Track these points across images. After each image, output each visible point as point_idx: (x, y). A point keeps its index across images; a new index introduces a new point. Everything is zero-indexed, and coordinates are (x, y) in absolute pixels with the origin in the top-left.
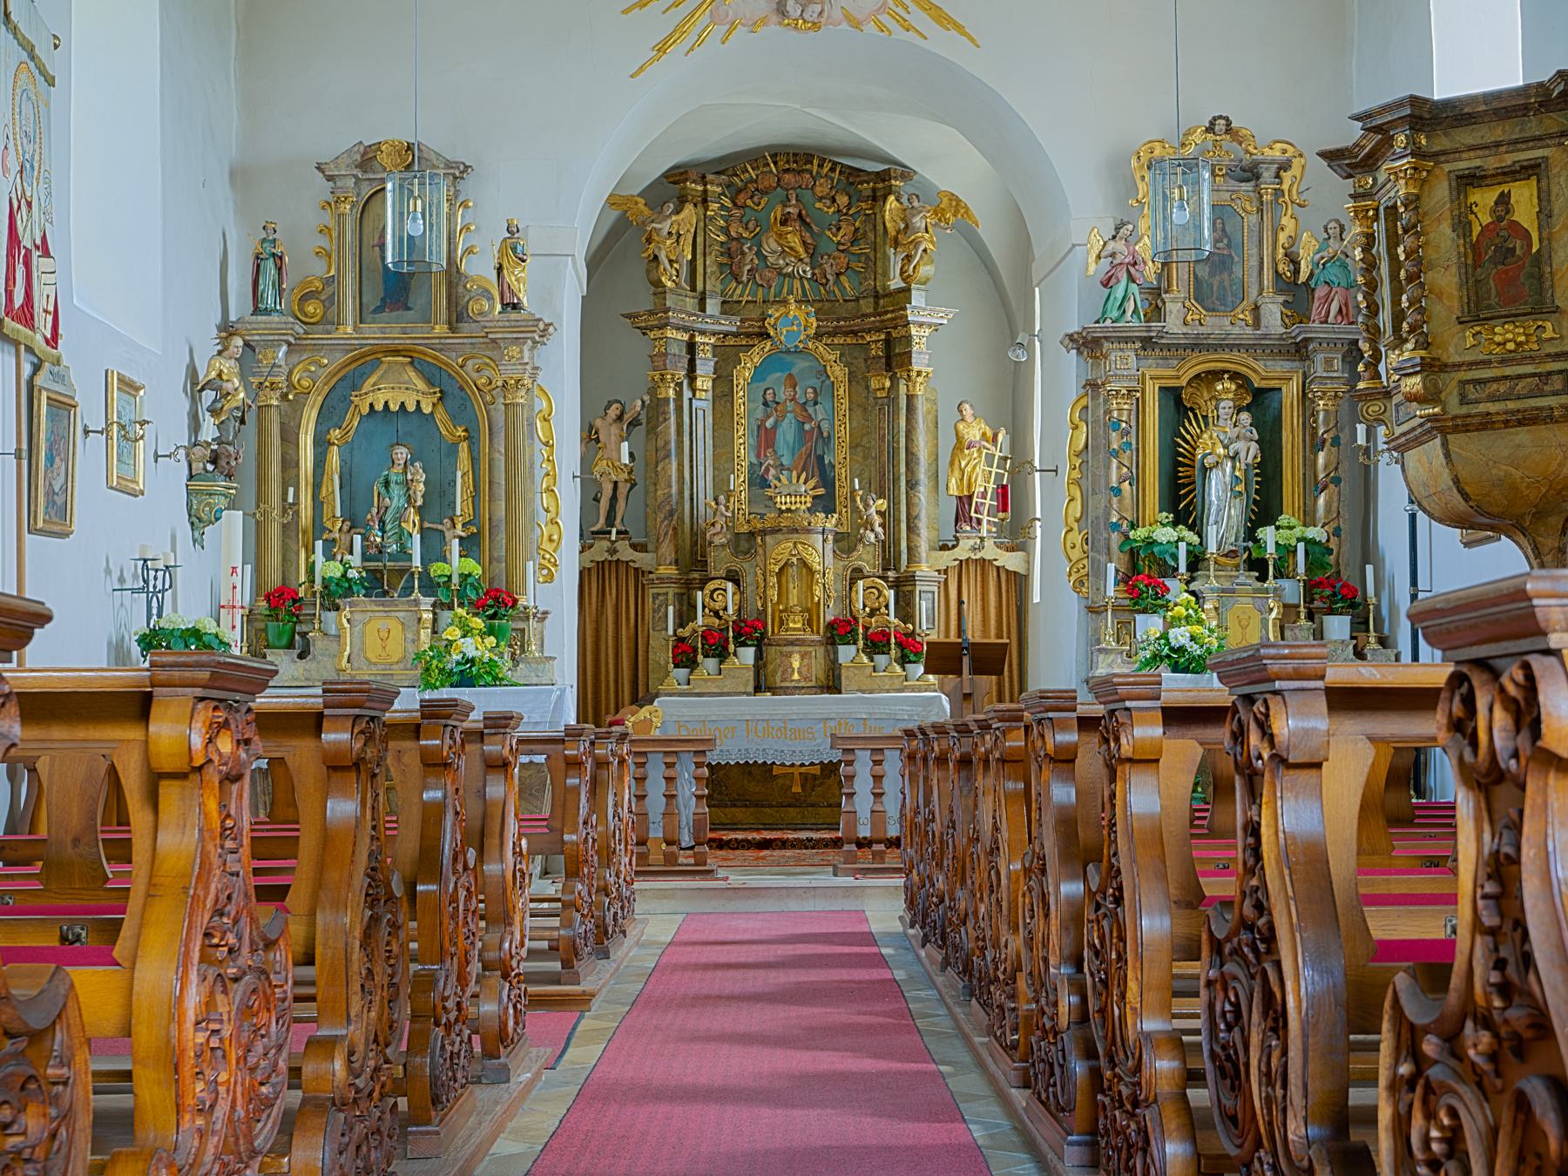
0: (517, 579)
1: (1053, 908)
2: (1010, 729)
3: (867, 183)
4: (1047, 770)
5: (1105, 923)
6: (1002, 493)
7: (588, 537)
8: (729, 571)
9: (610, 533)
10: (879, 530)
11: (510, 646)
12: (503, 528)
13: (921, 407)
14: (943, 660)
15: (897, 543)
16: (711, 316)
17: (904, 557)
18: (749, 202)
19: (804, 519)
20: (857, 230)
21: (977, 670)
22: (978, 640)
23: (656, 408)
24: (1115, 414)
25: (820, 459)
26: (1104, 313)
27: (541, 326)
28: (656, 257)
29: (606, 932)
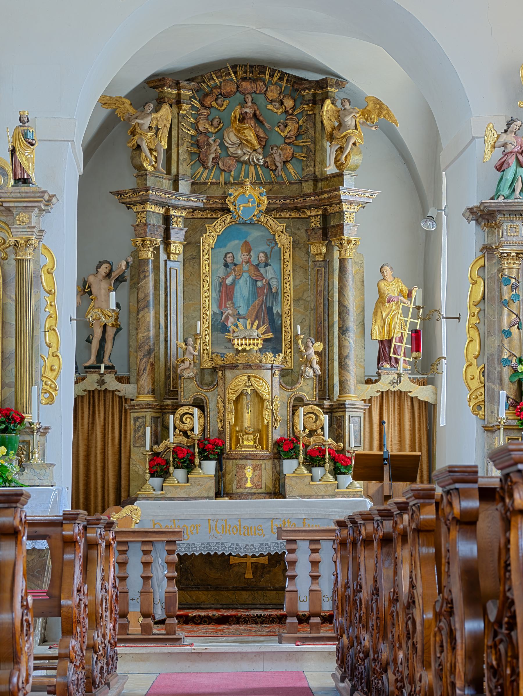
0: (24, 401)
1: (459, 641)
2: (424, 505)
3: (309, 90)
4: (455, 532)
5: (502, 647)
6: (416, 335)
7: (82, 371)
8: (195, 399)
9: (99, 368)
10: (317, 367)
11: (18, 455)
12: (13, 359)
13: (351, 269)
14: (369, 469)
15: (331, 377)
16: (183, 195)
17: (337, 389)
18: (214, 104)
19: (256, 358)
20: (300, 127)
21: (395, 477)
22: (396, 452)
23: (137, 268)
24: (506, 272)
25: (270, 310)
26: (498, 191)
27: (46, 197)
28: (139, 147)
29: (94, 683)
